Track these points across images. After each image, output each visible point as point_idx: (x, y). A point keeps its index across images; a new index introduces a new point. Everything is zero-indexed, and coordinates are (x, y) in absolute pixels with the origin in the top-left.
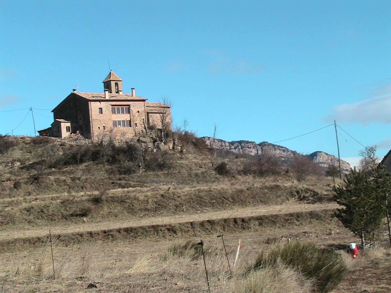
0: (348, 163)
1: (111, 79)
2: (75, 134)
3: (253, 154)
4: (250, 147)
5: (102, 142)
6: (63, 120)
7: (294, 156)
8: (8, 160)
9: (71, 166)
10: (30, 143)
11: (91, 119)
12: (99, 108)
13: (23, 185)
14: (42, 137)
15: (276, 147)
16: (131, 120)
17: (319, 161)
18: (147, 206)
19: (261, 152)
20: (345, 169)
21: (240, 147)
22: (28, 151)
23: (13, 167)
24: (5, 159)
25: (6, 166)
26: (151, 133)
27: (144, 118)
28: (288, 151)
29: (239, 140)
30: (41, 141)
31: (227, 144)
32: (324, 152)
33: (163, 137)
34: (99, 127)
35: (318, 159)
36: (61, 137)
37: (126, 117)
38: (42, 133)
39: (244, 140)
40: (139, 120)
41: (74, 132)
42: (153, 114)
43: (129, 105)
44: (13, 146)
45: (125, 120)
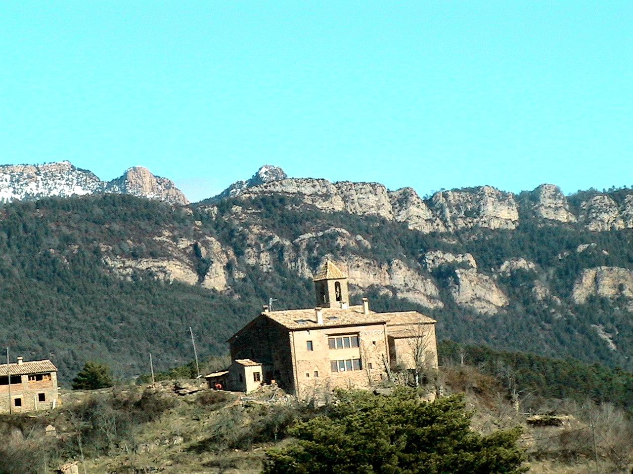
1: (327, 278)
2: (269, 386)
5: (312, 402)
6: (248, 360)
8: (163, 435)
9: (265, 444)
10: (195, 403)
11: (293, 361)
12: (308, 342)
14: (215, 391)
16: (362, 357)
18: (586, 315)
22: (194, 417)
23: (173, 445)
24: (158, 431)
25: (161, 444)
26: (397, 378)
27: (384, 353)
30: (213, 398)
33: (418, 384)
34: (308, 375)
36: (246, 391)
37: (352, 353)
38: (212, 381)
40: (376, 358)
42: (402, 339)
43: (357, 333)
44: (168, 408)
45: (352, 358)
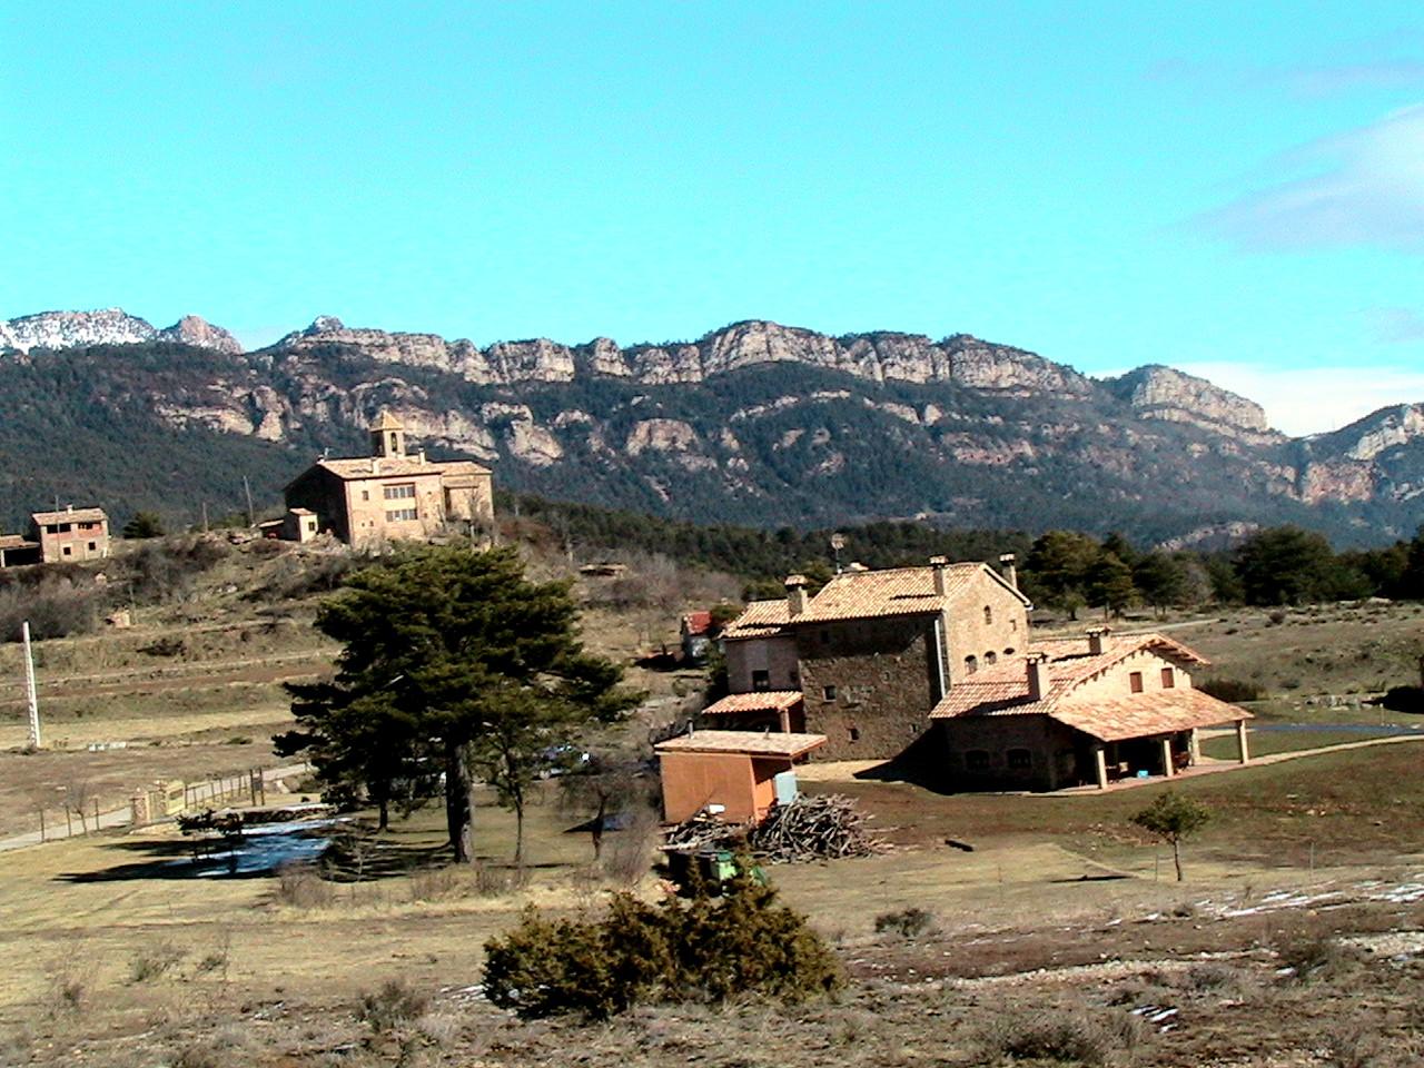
0: (1256, 405)
3: (918, 378)
4: (907, 353)
7: (1065, 384)
13: (255, 637)
15: (1001, 353)
17: (1153, 399)
19: (947, 371)
20: (1246, 426)
21: (873, 355)
28: (1044, 368)
29: (871, 331)
31: (829, 346)
32: (1172, 367)
35: (1149, 393)
37: (409, 503)
39: (889, 330)
41: (322, 530)
